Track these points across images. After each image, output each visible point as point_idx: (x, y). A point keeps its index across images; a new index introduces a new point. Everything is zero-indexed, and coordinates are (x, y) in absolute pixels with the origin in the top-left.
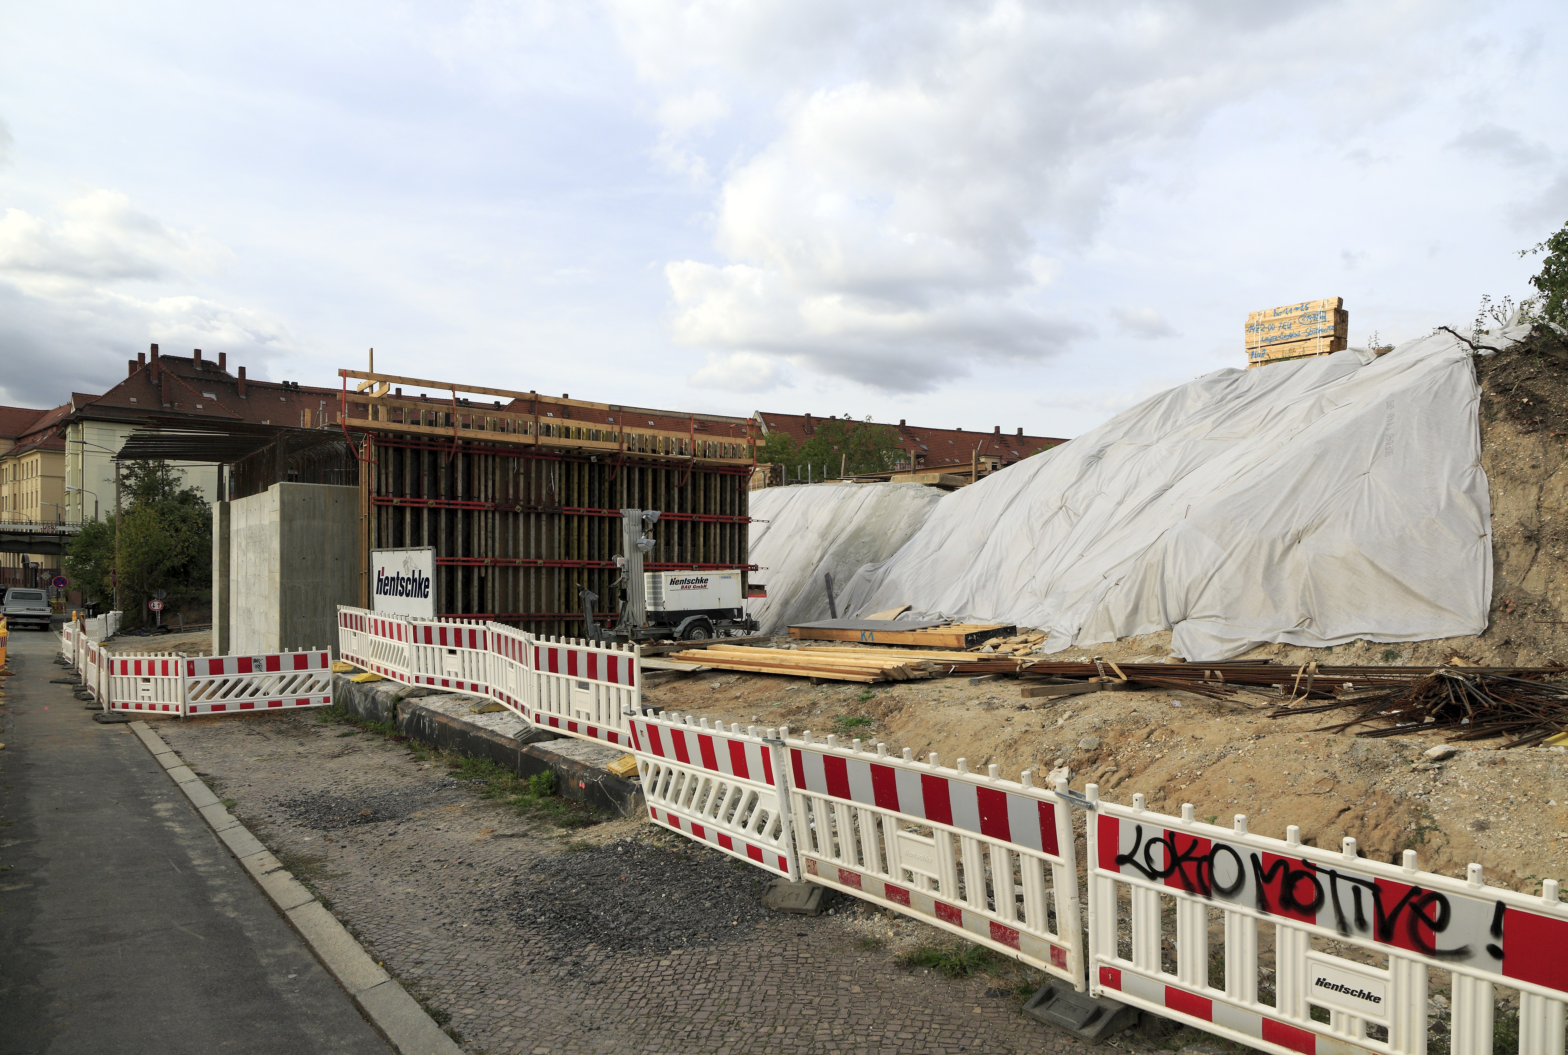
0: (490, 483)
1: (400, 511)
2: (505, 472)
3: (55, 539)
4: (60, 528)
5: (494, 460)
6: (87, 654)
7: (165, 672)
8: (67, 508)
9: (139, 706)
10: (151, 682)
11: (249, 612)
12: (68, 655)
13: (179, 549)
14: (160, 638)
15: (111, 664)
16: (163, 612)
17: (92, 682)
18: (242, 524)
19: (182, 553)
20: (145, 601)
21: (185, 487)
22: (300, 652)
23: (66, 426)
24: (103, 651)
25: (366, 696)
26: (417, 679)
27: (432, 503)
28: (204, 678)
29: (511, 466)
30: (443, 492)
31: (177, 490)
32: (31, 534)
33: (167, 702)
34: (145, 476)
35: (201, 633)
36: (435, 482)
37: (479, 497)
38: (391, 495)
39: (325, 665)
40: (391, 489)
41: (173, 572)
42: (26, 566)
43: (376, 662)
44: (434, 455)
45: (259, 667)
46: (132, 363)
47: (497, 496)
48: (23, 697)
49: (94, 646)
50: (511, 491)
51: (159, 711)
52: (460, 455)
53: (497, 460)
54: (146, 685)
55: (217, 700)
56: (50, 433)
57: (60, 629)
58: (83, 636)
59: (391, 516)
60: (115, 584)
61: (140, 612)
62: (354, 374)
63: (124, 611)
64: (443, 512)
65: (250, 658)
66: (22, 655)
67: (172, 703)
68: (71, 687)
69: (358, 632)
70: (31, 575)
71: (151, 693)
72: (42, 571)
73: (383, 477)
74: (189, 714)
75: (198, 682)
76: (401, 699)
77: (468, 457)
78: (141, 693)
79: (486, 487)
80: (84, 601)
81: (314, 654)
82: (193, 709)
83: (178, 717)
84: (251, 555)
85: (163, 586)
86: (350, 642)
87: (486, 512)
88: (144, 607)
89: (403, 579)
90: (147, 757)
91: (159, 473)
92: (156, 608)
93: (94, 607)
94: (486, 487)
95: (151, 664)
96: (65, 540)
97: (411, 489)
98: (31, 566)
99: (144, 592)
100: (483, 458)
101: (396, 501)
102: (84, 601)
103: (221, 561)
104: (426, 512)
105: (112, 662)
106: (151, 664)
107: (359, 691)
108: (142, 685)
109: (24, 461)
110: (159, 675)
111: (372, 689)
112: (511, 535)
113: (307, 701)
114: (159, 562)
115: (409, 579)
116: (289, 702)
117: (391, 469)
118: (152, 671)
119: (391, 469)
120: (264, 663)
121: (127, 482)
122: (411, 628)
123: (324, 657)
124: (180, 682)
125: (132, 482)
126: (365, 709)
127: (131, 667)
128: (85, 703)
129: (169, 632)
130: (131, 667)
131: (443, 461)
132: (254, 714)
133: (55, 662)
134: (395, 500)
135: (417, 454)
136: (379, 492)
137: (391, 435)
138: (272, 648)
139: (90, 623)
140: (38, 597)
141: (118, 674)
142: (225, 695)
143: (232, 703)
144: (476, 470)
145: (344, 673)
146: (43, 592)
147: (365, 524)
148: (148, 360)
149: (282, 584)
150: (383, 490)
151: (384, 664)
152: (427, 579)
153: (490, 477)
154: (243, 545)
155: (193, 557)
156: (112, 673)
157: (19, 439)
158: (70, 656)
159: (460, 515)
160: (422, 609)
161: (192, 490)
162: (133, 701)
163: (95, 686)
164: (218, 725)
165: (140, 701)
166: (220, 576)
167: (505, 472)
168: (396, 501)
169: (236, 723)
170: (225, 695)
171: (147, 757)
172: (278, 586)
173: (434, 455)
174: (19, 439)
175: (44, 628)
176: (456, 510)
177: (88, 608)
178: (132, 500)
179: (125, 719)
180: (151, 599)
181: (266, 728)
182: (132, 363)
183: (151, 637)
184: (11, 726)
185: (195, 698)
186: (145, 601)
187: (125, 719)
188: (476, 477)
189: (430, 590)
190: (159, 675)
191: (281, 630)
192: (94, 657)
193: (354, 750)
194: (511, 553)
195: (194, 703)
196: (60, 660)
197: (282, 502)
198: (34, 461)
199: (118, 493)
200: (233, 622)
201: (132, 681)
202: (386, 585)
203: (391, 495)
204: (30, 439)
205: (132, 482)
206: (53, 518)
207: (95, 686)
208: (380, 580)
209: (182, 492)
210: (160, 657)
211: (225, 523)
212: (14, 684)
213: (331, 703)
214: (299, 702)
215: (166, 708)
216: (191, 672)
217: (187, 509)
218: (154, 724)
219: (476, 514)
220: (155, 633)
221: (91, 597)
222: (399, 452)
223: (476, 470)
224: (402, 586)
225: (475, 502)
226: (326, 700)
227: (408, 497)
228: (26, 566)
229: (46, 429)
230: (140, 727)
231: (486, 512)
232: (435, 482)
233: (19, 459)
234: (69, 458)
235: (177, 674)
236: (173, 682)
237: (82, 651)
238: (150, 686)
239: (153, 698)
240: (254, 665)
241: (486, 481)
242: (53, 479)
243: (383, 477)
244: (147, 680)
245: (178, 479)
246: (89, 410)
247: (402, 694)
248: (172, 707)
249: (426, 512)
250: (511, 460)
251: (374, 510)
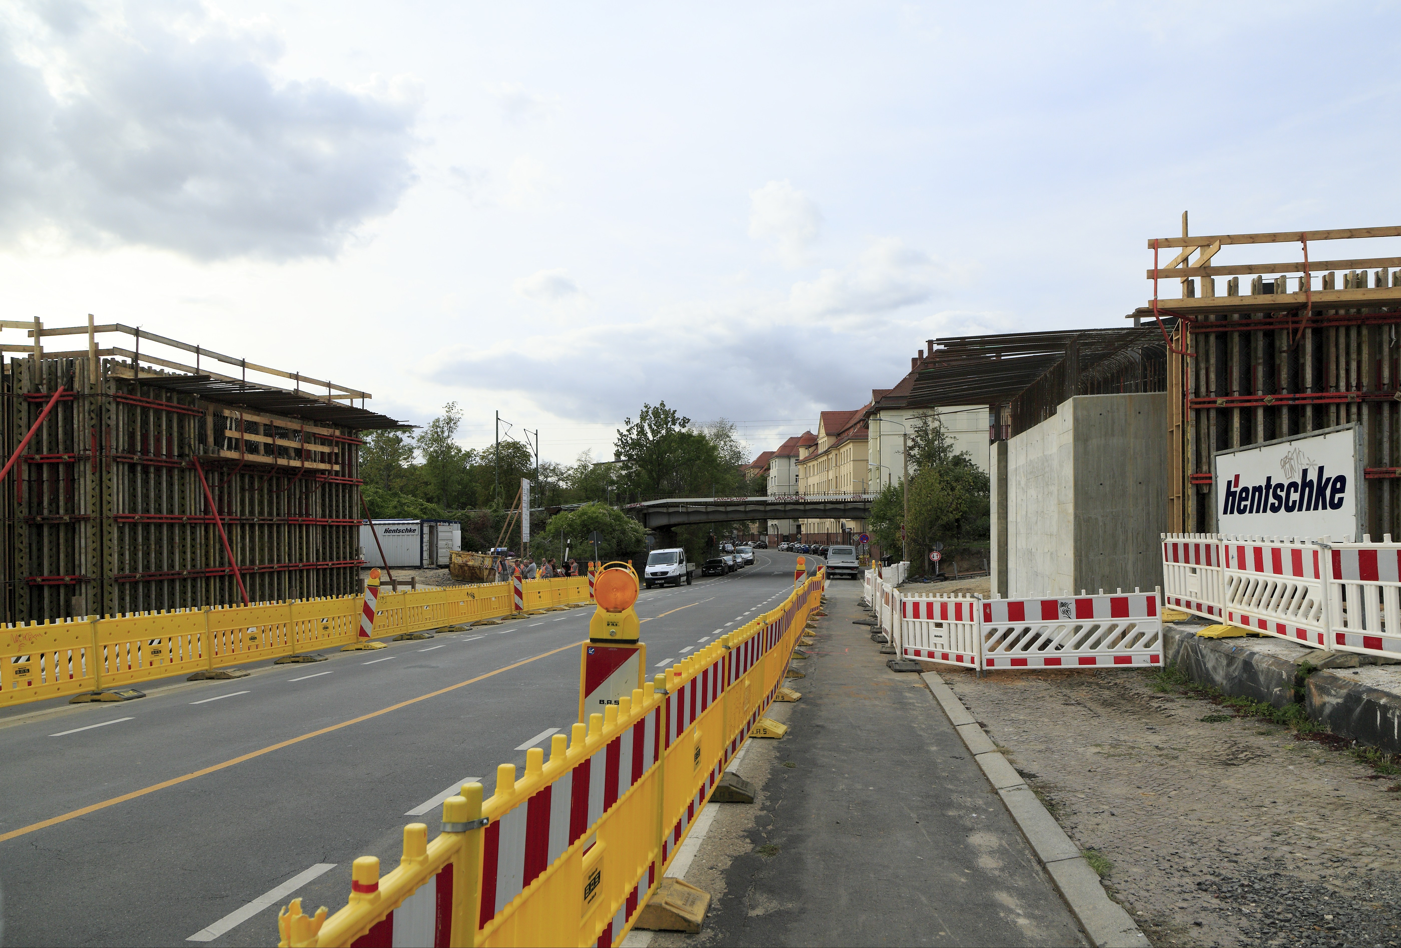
0: (1354, 365)
1: (1225, 414)
2: (1376, 348)
3: (861, 506)
4: (864, 496)
5: (1359, 334)
6: (882, 596)
7: (959, 617)
8: (870, 483)
9: (931, 655)
10: (944, 628)
11: (1030, 554)
12: (868, 598)
13: (954, 506)
14: (939, 584)
15: (904, 605)
16: (941, 561)
17: (886, 625)
18: (1022, 461)
19: (957, 509)
20: (927, 552)
21: (957, 453)
22: (1119, 594)
23: (868, 417)
24: (896, 592)
25: (1231, 659)
26: (1340, 638)
27: (1269, 399)
28: (1002, 624)
29: (1386, 337)
30: (1284, 383)
31: (951, 455)
32: (845, 502)
33: (961, 652)
34: (926, 445)
35: (973, 580)
36: (1272, 372)
37: (1337, 386)
38: (1213, 395)
39: (1151, 611)
40: (1213, 388)
41: (947, 527)
42: (844, 531)
43: (1239, 609)
44: (1270, 336)
45: (1067, 612)
46: (914, 360)
47: (1365, 381)
48: (829, 637)
49: (888, 587)
50: (1386, 373)
51: (952, 662)
52: (1309, 333)
53: (1365, 332)
54: (938, 631)
55: (1017, 652)
56: (858, 426)
57: (863, 577)
58: (879, 580)
59: (1213, 421)
60: (904, 537)
61: (923, 561)
62: (1168, 243)
63: (911, 561)
64: (1285, 411)
65: (1055, 602)
66: (836, 599)
67: (967, 654)
68: (869, 628)
69: (1203, 566)
70: (847, 536)
71: (944, 640)
72: (854, 534)
73: (1203, 373)
74: (985, 667)
75: (995, 630)
76: (1312, 670)
77: (1319, 333)
78: (934, 639)
79: (1348, 371)
80: (882, 554)
81: (1137, 598)
82: (990, 662)
83: (973, 670)
84: (1032, 492)
85: (942, 539)
86: (1180, 581)
87: (1348, 406)
88: (926, 558)
89: (1280, 486)
90: (946, 728)
91: (936, 443)
92: (936, 558)
93: (888, 559)
94: (1348, 371)
95: (944, 607)
96: (868, 505)
97: (1240, 384)
98: (847, 530)
99: (925, 545)
100: (1342, 332)
101: (1220, 401)
102: (882, 554)
103: (999, 503)
104: (1260, 413)
105: (905, 603)
106: (944, 607)
107: (1214, 650)
108: (934, 631)
109: (842, 451)
110: (952, 620)
111: (1241, 650)
112: (1386, 434)
113: (1128, 660)
114: (938, 518)
115: (1293, 485)
116: (1105, 658)
117: (1213, 361)
118: (944, 616)
119: (1213, 361)
120: (1073, 607)
121: (912, 453)
122: (1329, 555)
123: (1151, 601)
124: (975, 629)
125: (915, 452)
126: (1228, 676)
127: (923, 610)
128: (880, 645)
129: (946, 579)
130: (923, 610)
131: (1283, 343)
132: (1061, 671)
133: (859, 605)
134: (1219, 401)
135: (1247, 339)
136: (1197, 393)
137: (1212, 317)
138: (1064, 591)
139: (886, 571)
140: (849, 552)
141: (910, 618)
142: (1026, 648)
143: (1035, 659)
144: (1333, 350)
145: (1177, 623)
146: (853, 548)
147: (1177, 436)
148: (925, 355)
149: (1076, 516)
150: (1203, 389)
151: (1255, 613)
152: (1342, 479)
153: (1354, 356)
154: (1023, 483)
155: (965, 512)
156: (905, 617)
157: (839, 435)
158: (870, 599)
159: (1309, 412)
160: (1340, 526)
161: (962, 454)
162: (925, 649)
163: (889, 630)
164: (1020, 684)
165: (932, 649)
166: (999, 518)
167: (1376, 348)
168: (1220, 401)
169: (1043, 684)
170: (1026, 648)
171: (946, 728)
172: (1071, 518)
173: (1270, 336)
174: (839, 435)
175: (854, 577)
176: (1304, 407)
177: (884, 560)
178: (916, 467)
179: (918, 668)
180: (931, 550)
181: (1081, 694)
182: (914, 360)
183: (932, 584)
184: (812, 670)
185: (992, 649)
186: (927, 552)
187: (917, 668)
188: (1333, 358)
189: (1349, 496)
190: (952, 620)
191: (1076, 570)
192: (887, 598)
193: (1256, 756)
194: (1386, 460)
195: (991, 655)
196: (862, 604)
197: (1076, 420)
198: (849, 449)
199: (906, 462)
200: (1011, 565)
201: (924, 625)
202: (1241, 499)
203: (1213, 395)
204: (846, 434)
205: (915, 452)
206: (861, 490)
207: (889, 630)
208: (1229, 494)
209: (955, 457)
210: (953, 599)
211: (1003, 464)
212: (825, 624)
213: (1161, 664)
214: (1118, 660)
215: (960, 658)
216: (988, 618)
217: (958, 470)
218: (948, 677)
219: (1333, 409)
220: (935, 580)
221: (886, 550)
222: (1223, 338)
223: (1333, 350)
224: (1276, 496)
225: (1332, 392)
226: (1154, 659)
227: (1236, 394)
228: (844, 531)
229: (856, 424)
230: (932, 678)
231: (1348, 406)
232: (1272, 372)
233: (839, 449)
234: (871, 441)
235: (972, 620)
236: (967, 628)
237: (878, 594)
238: (943, 631)
239: (946, 646)
240: (1060, 610)
241: (1348, 364)
242: (861, 461)
243: (1203, 373)
244: (939, 625)
245: (951, 446)
246: (885, 401)
247: (1313, 660)
248: (967, 658)
249: (1260, 413)
250: (1386, 329)
251: (1191, 415)
